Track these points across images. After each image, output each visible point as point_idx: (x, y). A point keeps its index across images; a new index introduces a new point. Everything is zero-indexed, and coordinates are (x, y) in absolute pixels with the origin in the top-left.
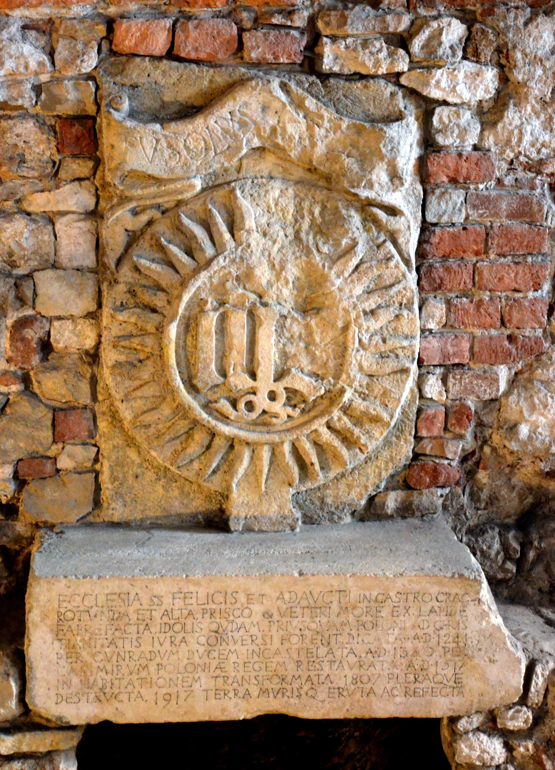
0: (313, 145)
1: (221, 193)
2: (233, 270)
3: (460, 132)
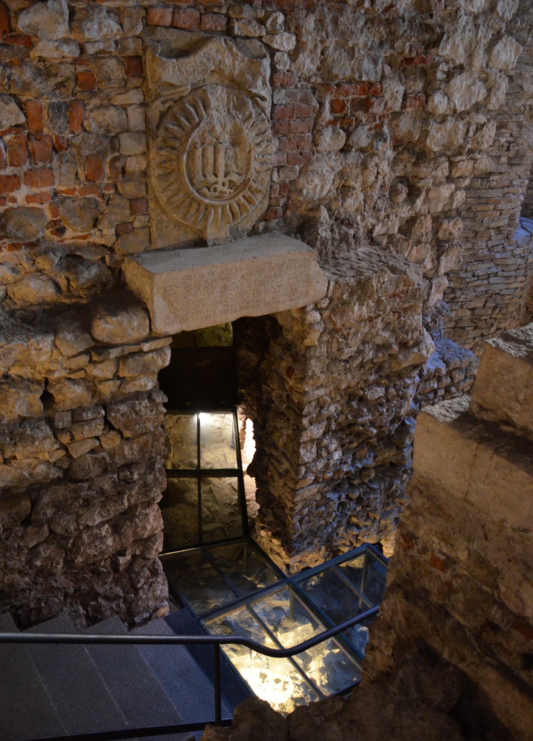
0: (234, 69)
1: (199, 92)
2: (207, 128)
3: (284, 63)
